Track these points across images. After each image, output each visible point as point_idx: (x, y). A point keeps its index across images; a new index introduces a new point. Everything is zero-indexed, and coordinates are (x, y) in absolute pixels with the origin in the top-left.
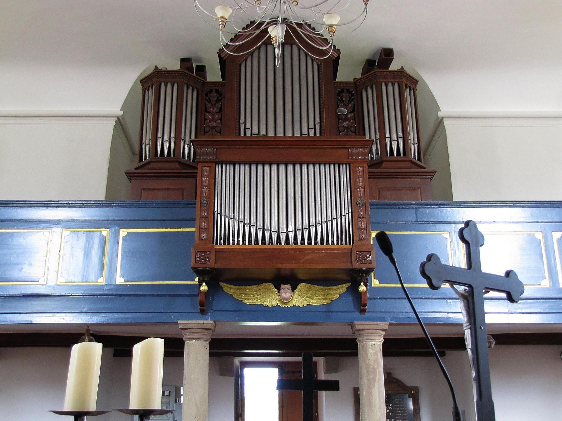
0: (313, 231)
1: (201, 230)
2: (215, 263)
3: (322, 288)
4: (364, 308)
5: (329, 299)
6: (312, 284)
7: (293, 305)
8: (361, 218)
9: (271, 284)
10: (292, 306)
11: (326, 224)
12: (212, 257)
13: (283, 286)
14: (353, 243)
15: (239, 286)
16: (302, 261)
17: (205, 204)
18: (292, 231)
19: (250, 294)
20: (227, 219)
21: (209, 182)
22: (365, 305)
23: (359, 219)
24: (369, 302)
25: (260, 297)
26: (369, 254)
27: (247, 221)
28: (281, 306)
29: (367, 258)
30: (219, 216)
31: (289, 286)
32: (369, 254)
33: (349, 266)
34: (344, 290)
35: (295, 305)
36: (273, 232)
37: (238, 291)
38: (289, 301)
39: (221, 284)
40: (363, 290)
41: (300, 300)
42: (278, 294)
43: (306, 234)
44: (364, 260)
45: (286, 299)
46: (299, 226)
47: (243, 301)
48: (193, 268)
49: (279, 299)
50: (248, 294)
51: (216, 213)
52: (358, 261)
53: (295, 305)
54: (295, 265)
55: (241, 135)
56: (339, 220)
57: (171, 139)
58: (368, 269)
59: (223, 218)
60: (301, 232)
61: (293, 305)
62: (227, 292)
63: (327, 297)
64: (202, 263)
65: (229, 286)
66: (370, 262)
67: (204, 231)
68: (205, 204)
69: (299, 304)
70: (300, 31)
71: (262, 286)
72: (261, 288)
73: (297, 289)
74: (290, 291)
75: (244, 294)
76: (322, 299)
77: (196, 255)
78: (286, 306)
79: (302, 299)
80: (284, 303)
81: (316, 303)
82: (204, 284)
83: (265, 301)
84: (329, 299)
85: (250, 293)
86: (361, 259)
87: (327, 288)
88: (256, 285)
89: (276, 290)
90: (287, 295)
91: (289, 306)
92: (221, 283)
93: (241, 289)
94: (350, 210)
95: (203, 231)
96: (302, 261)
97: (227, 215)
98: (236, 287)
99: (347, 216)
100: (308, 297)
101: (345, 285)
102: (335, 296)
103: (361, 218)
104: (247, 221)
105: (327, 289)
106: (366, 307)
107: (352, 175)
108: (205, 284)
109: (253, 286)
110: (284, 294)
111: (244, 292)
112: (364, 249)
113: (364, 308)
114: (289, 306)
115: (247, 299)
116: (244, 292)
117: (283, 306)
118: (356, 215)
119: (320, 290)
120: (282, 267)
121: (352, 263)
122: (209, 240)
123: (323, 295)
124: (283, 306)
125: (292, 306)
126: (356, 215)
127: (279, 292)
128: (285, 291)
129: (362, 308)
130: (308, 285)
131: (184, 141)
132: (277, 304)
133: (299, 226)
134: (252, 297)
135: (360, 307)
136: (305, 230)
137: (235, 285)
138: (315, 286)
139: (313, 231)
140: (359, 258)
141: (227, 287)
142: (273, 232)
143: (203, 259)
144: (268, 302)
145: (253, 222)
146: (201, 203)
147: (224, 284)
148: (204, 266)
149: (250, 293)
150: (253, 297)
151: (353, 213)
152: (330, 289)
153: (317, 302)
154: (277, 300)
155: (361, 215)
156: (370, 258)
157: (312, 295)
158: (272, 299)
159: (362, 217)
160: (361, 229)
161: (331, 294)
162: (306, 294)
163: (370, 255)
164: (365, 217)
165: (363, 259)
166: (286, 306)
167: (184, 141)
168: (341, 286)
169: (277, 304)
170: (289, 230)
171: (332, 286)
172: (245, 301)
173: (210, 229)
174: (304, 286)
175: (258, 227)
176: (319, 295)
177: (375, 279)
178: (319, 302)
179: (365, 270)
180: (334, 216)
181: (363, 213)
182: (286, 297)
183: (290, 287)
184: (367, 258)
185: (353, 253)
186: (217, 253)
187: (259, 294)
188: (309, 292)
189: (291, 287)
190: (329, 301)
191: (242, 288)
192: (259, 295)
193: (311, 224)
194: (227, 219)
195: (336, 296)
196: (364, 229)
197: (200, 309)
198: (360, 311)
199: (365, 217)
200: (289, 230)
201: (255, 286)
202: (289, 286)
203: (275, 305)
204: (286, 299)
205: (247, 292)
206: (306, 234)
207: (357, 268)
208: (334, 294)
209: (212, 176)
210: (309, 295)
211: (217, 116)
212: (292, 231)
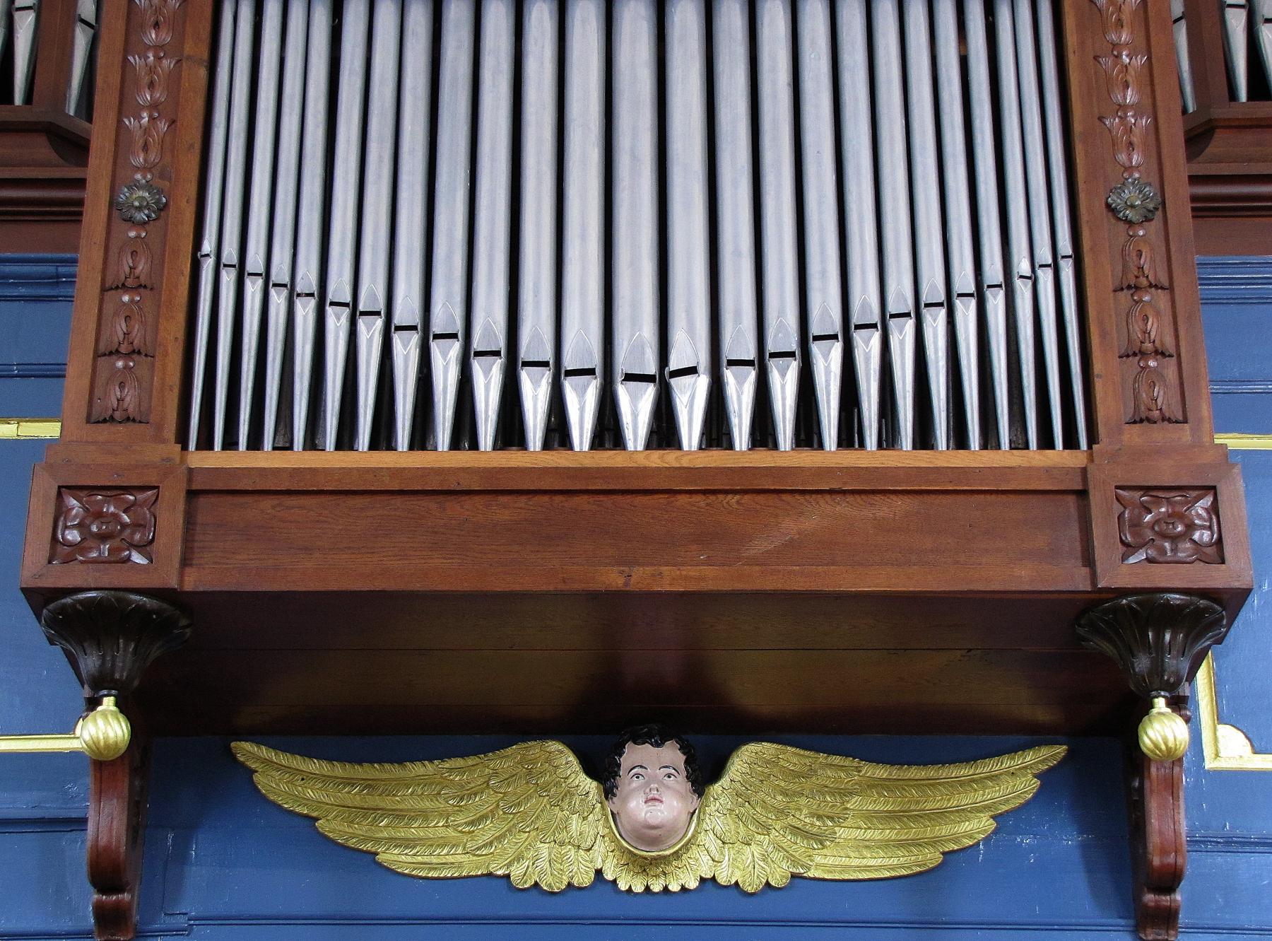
0: (827, 364)
1: (102, 361)
2: (186, 562)
3: (881, 772)
4: (1165, 900)
5: (934, 842)
6: (818, 751)
7: (702, 880)
8: (1137, 288)
9: (561, 747)
10: (693, 884)
11: (910, 324)
12: (171, 519)
13: (634, 755)
14: (1093, 438)
15: (360, 762)
16: (760, 546)
17: (139, 209)
18: (692, 371)
19: (425, 815)
20: (278, 300)
21: (174, 79)
22: (1169, 880)
23: (1124, 296)
24: (1194, 865)
25: (488, 830)
26: (1207, 501)
27: (407, 308)
28: (623, 886)
29: (1191, 527)
30: (228, 278)
31: (671, 754)
32: (1207, 501)
33: (1073, 579)
34: (1026, 786)
35: (714, 879)
36: (570, 373)
37: (353, 796)
38: (677, 855)
39: (247, 750)
40: (1171, 744)
41: (747, 849)
43: (783, 387)
44: (1175, 539)
45: (650, 835)
46: (738, 340)
47: (380, 858)
48: (39, 598)
49: (613, 840)
50: (414, 810)
51: (208, 267)
52: (1130, 548)
53: (714, 879)
54: (708, 571)
55: (482, 450)
56: (996, 303)
57: (17, 15)
58: (1203, 603)
59: (253, 290)
60: (752, 374)
61: (702, 880)
62: (279, 800)
63: (914, 831)
64: (94, 561)
65: (297, 762)
66: (1217, 551)
67: (126, 367)
68: (139, 209)
69: (737, 877)
71: (507, 760)
73: (725, 781)
74: (680, 783)
75: (386, 812)
76: (886, 845)
77: (60, 511)
78: (657, 888)
79: (760, 844)
80: (644, 866)
82: (108, 703)
84: (934, 842)
85: (427, 804)
86: (1150, 535)
87: (914, 772)
88: (462, 756)
89: (590, 786)
91: (674, 887)
92: (247, 746)
93: (370, 785)
94: (1065, 246)
95: (115, 371)
96: (760, 546)
97: (280, 271)
98: (339, 770)
99: (1046, 278)
100: (796, 830)
101: (1030, 757)
102: (966, 827)
103: (1137, 288)
104: (407, 308)
105: (918, 784)
106: (1178, 897)
107: (1071, 39)
108: (117, 704)
109: (448, 764)
110: (641, 800)
111: (387, 803)
112: (1165, 473)
113: (1165, 900)
114: (674, 887)
115: (408, 843)
116: (387, 803)
117: (638, 888)
118: (1102, 275)
119: (871, 787)
120: (626, 584)
121: (1088, 560)
122: (152, 418)
123: (891, 817)
124: (638, 888)
125: (693, 884)
126: (1102, 275)
127: (609, 792)
128: (648, 784)
129: (1150, 898)
130: (792, 757)
131: (91, 32)
132: (599, 873)
133: (738, 340)
134: (437, 828)
135: (1137, 898)
136: (781, 361)
137: (330, 759)
138: (837, 760)
139: (827, 364)
140: (1136, 524)
141: (279, 767)
142: (570, 373)
143: (103, 537)
145: (446, 313)
146: (113, 204)
147: (264, 752)
148: (115, 577)
149: (427, 804)
150: (441, 832)
151: (1088, 259)
152: (933, 784)
153: (856, 862)
154: (601, 848)
155: (1141, 268)
156: (1210, 528)
157: (819, 817)
158: (562, 844)
159: (1144, 282)
160: (1143, 354)
161: (941, 815)
162: (781, 813)
163: (1214, 509)
164: (1164, 281)
165: (1164, 536)
166: (657, 888)
167: (91, 32)
168: (1007, 763)
169: (599, 873)
170: (674, 365)
171: (943, 762)
172: (391, 856)
173: (166, 354)
174: (768, 762)
175: (477, 345)
176: (871, 818)
177: (1221, 718)
178: (865, 862)
179: (1180, 608)
180: (964, 279)
181: (1153, 260)
184: (1191, 527)
185: (1095, 498)
186: (202, 501)
188: (803, 801)
190: (932, 857)
191: (377, 775)
192: (484, 817)
193: (815, 329)
194: (278, 300)
195: (979, 826)
196: (1163, 354)
197: (100, 911)
198: (1131, 922)
199: (1164, 281)
200: (674, 365)
201: (459, 762)
202: (671, 754)
203: (585, 879)
204: (654, 832)
205: (406, 800)
206: (783, 387)
207: (1124, 592)
208: (963, 813)
209: (196, 48)
210: (804, 819)
212: (692, 371)
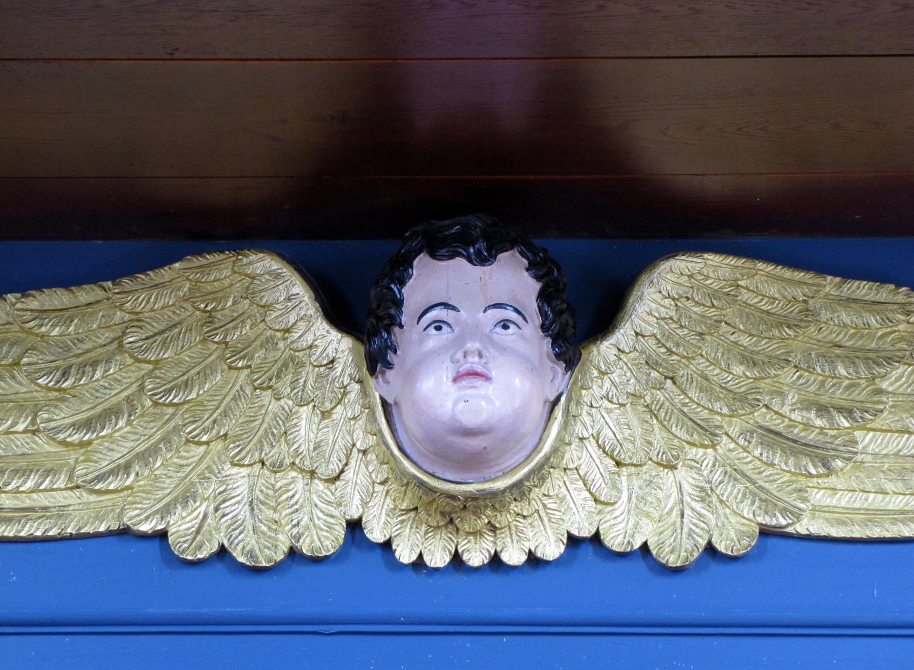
7: (573, 541)
10: (552, 550)
28: (405, 554)
35: (596, 538)
41: (668, 478)
42: (364, 393)
49: (387, 460)
53: (596, 538)
61: (573, 541)
70: (199, 513)
72: (137, 321)
78: (476, 557)
81: (873, 516)
83: (186, 497)
90: (483, 388)
91: (514, 556)
114: (514, 556)
117: (438, 558)
124: (438, 558)
125: (552, 550)
128: (458, 342)
132: (355, 527)
138: (862, 289)
144: (238, 509)
157: (822, 410)
158: (277, 468)
166: (476, 557)
169: (355, 527)
174: (714, 295)
182: (470, 420)
183: (534, 287)
187: (117, 396)
188: (788, 376)
189: (543, 296)
192: (113, 413)
211: (857, 217)
